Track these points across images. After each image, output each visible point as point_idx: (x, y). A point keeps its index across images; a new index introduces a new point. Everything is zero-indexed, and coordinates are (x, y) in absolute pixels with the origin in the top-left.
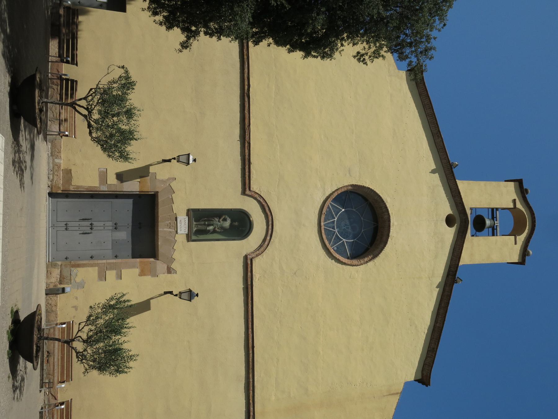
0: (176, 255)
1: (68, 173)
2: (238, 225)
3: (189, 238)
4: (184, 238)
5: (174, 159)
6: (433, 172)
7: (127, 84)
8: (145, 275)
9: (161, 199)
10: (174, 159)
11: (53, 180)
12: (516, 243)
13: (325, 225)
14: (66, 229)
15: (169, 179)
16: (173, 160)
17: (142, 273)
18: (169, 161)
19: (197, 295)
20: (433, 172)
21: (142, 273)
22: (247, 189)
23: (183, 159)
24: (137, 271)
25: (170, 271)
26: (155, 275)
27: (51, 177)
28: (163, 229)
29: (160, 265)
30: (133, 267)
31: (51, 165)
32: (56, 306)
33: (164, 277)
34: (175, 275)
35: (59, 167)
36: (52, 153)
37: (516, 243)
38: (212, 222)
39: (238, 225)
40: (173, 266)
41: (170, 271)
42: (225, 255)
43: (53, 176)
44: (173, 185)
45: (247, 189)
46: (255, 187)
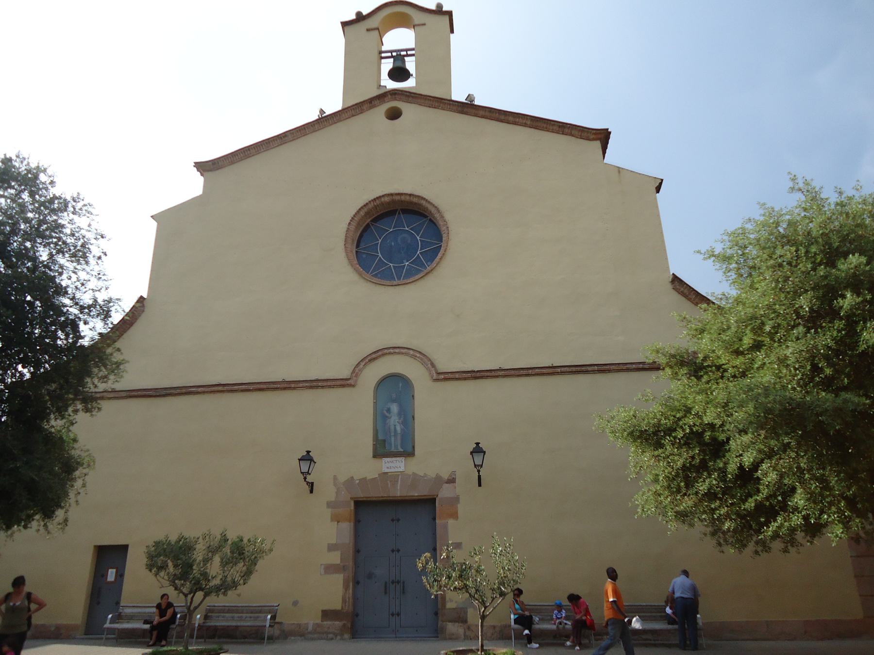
0: (432, 474)
1: (327, 614)
2: (395, 388)
3: (408, 453)
4: (412, 461)
5: (305, 478)
6: (322, 112)
7: (759, 203)
8: (457, 513)
9: (361, 495)
10: (305, 478)
11: (334, 634)
12: (424, 24)
13: (399, 279)
14: (398, 614)
15: (335, 485)
16: (310, 479)
17: (455, 515)
18: (311, 485)
19: (478, 444)
20: (322, 112)
21: (455, 515)
22: (348, 382)
23: (305, 467)
24: (451, 522)
25: (452, 481)
26: (456, 499)
27: (330, 636)
28: (399, 491)
29: (445, 492)
30: (445, 527)
31: (316, 636)
32: (494, 627)
33: (459, 488)
34: (457, 474)
35: (318, 625)
36: (301, 636)
37: (424, 24)
38: (392, 428)
39: (395, 388)
40: (446, 476)
41: (452, 481)
42: (431, 406)
43: (330, 633)
44: (342, 478)
45: (348, 382)
46: (345, 373)
